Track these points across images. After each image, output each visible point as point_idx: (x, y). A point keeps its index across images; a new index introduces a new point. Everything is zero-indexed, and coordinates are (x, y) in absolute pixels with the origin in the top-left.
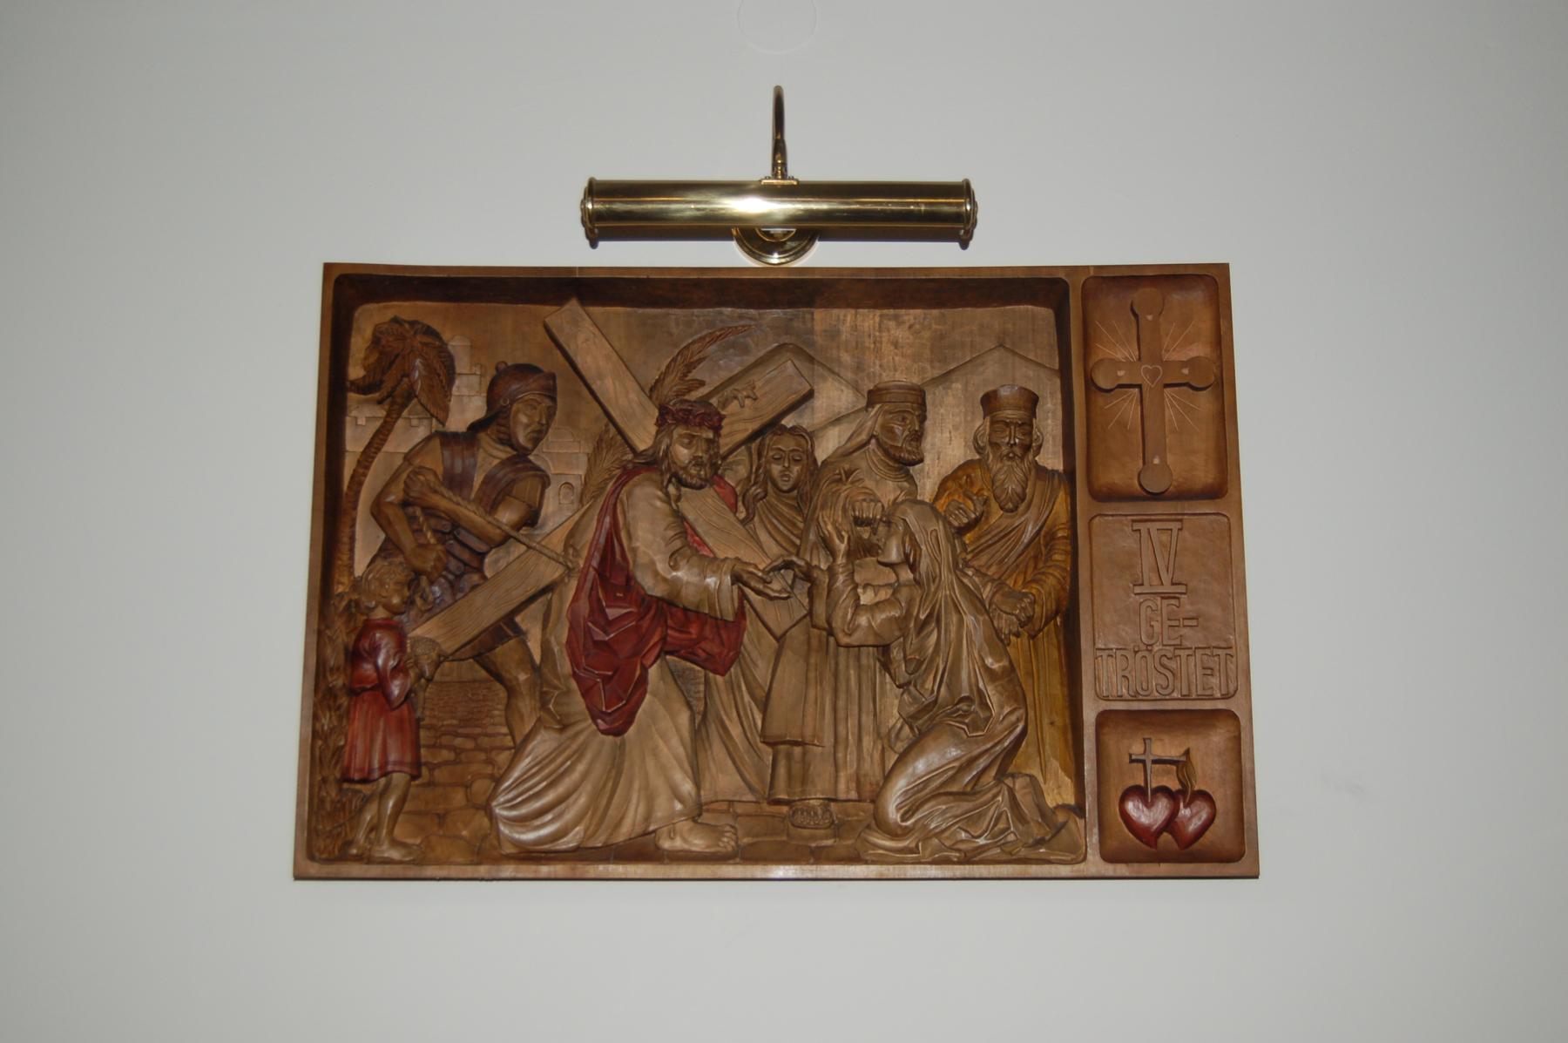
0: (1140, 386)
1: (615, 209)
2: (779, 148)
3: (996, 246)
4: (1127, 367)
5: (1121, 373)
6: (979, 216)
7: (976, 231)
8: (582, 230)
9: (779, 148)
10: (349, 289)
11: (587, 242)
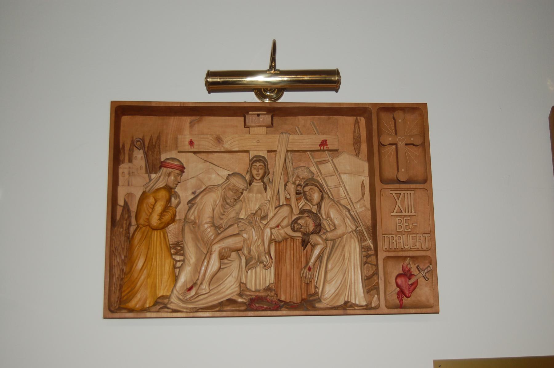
1: (219, 81)
4: (393, 137)
6: (342, 81)
8: (205, 88)
10: (121, 111)
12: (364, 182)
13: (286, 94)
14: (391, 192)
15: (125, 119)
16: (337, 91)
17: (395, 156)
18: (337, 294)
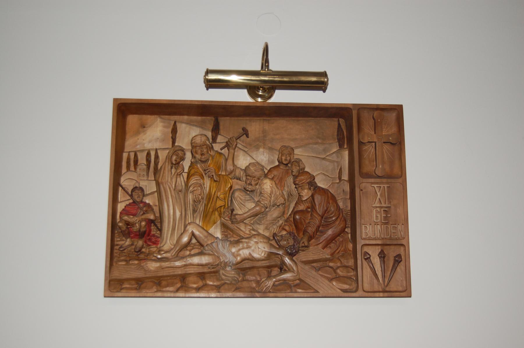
0: (375, 142)
3: (337, 94)
4: (370, 135)
6: (329, 82)
7: (328, 87)
8: (204, 85)
13: (277, 92)
14: (373, 185)
15: (132, 120)
16: (324, 91)
17: (370, 247)
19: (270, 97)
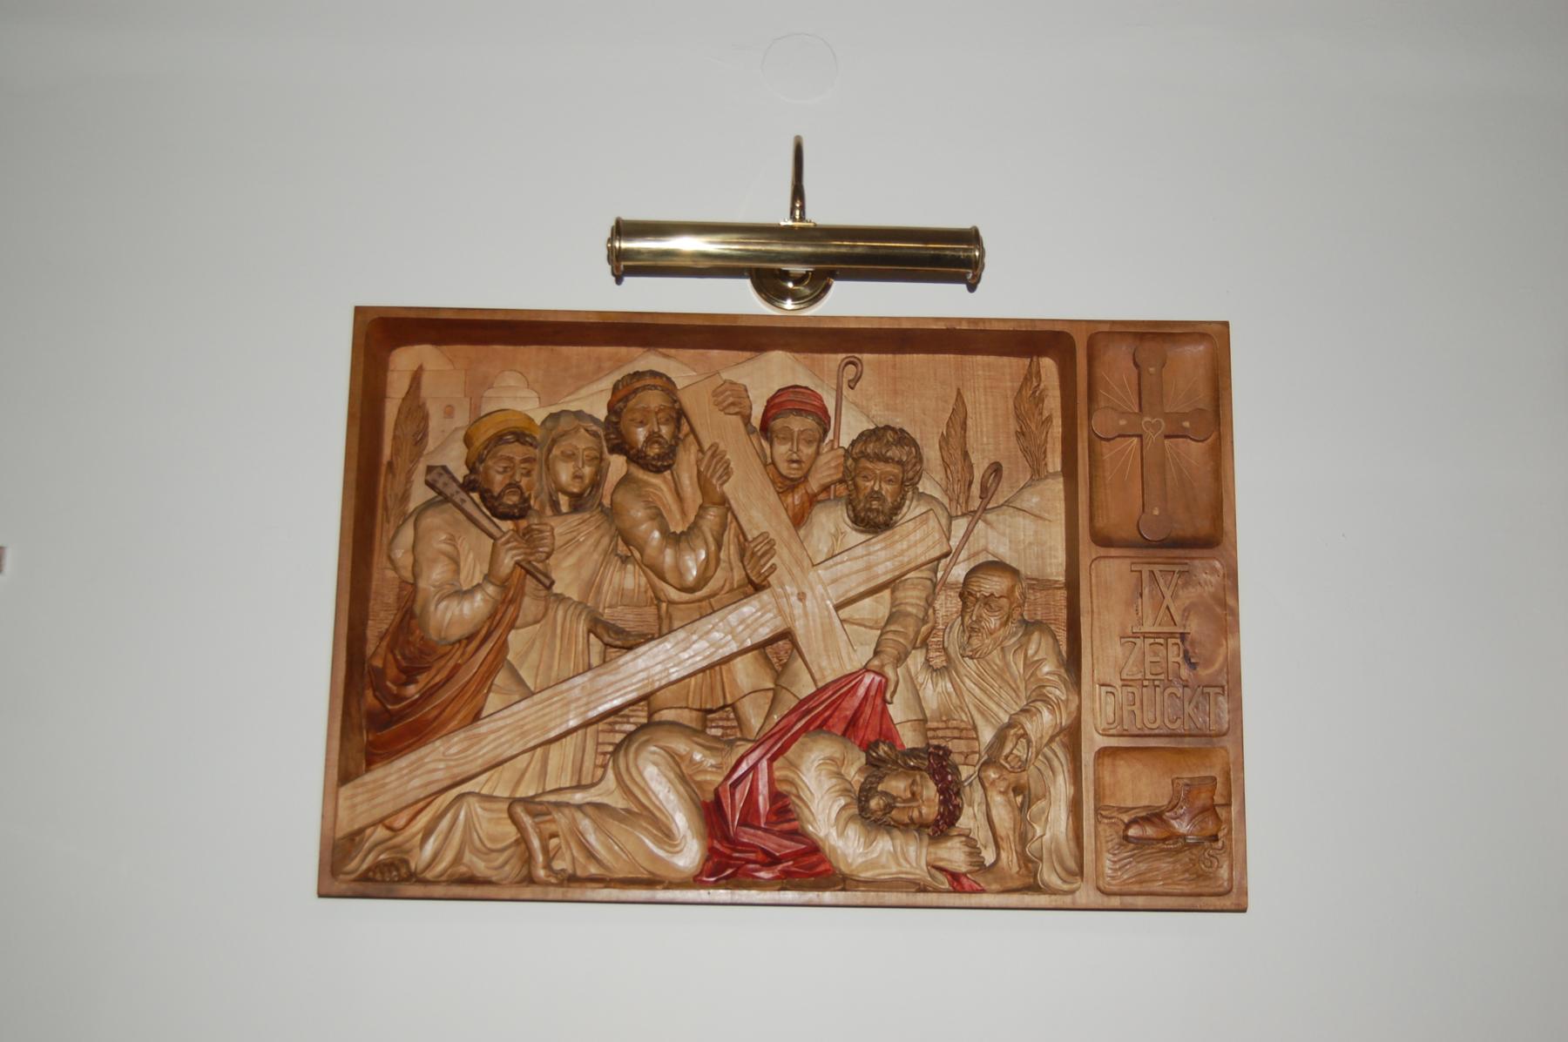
2: (798, 193)
3: (997, 298)
4: (1136, 423)
5: (1123, 422)
6: (987, 260)
7: (984, 275)
8: (608, 268)
9: (798, 193)
11: (613, 279)
12: (426, 390)
13: (837, 286)
15: (404, 360)
16: (972, 288)
18: (833, 702)
19: (815, 299)
